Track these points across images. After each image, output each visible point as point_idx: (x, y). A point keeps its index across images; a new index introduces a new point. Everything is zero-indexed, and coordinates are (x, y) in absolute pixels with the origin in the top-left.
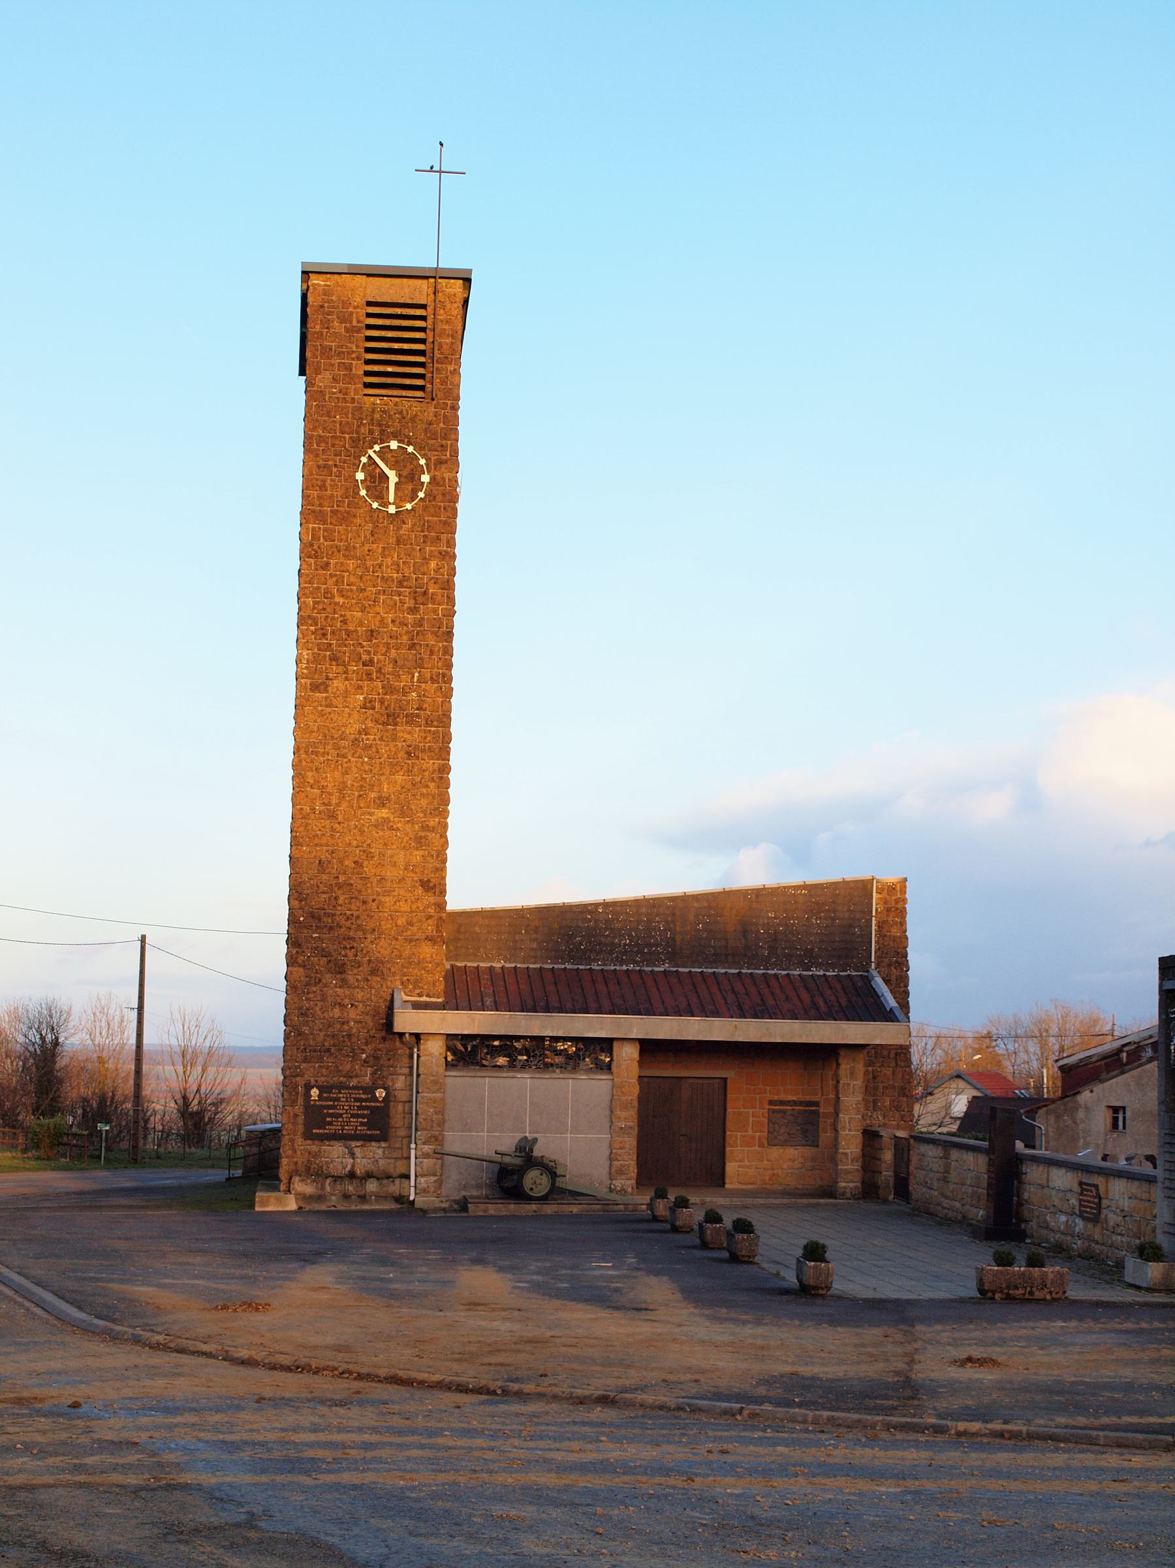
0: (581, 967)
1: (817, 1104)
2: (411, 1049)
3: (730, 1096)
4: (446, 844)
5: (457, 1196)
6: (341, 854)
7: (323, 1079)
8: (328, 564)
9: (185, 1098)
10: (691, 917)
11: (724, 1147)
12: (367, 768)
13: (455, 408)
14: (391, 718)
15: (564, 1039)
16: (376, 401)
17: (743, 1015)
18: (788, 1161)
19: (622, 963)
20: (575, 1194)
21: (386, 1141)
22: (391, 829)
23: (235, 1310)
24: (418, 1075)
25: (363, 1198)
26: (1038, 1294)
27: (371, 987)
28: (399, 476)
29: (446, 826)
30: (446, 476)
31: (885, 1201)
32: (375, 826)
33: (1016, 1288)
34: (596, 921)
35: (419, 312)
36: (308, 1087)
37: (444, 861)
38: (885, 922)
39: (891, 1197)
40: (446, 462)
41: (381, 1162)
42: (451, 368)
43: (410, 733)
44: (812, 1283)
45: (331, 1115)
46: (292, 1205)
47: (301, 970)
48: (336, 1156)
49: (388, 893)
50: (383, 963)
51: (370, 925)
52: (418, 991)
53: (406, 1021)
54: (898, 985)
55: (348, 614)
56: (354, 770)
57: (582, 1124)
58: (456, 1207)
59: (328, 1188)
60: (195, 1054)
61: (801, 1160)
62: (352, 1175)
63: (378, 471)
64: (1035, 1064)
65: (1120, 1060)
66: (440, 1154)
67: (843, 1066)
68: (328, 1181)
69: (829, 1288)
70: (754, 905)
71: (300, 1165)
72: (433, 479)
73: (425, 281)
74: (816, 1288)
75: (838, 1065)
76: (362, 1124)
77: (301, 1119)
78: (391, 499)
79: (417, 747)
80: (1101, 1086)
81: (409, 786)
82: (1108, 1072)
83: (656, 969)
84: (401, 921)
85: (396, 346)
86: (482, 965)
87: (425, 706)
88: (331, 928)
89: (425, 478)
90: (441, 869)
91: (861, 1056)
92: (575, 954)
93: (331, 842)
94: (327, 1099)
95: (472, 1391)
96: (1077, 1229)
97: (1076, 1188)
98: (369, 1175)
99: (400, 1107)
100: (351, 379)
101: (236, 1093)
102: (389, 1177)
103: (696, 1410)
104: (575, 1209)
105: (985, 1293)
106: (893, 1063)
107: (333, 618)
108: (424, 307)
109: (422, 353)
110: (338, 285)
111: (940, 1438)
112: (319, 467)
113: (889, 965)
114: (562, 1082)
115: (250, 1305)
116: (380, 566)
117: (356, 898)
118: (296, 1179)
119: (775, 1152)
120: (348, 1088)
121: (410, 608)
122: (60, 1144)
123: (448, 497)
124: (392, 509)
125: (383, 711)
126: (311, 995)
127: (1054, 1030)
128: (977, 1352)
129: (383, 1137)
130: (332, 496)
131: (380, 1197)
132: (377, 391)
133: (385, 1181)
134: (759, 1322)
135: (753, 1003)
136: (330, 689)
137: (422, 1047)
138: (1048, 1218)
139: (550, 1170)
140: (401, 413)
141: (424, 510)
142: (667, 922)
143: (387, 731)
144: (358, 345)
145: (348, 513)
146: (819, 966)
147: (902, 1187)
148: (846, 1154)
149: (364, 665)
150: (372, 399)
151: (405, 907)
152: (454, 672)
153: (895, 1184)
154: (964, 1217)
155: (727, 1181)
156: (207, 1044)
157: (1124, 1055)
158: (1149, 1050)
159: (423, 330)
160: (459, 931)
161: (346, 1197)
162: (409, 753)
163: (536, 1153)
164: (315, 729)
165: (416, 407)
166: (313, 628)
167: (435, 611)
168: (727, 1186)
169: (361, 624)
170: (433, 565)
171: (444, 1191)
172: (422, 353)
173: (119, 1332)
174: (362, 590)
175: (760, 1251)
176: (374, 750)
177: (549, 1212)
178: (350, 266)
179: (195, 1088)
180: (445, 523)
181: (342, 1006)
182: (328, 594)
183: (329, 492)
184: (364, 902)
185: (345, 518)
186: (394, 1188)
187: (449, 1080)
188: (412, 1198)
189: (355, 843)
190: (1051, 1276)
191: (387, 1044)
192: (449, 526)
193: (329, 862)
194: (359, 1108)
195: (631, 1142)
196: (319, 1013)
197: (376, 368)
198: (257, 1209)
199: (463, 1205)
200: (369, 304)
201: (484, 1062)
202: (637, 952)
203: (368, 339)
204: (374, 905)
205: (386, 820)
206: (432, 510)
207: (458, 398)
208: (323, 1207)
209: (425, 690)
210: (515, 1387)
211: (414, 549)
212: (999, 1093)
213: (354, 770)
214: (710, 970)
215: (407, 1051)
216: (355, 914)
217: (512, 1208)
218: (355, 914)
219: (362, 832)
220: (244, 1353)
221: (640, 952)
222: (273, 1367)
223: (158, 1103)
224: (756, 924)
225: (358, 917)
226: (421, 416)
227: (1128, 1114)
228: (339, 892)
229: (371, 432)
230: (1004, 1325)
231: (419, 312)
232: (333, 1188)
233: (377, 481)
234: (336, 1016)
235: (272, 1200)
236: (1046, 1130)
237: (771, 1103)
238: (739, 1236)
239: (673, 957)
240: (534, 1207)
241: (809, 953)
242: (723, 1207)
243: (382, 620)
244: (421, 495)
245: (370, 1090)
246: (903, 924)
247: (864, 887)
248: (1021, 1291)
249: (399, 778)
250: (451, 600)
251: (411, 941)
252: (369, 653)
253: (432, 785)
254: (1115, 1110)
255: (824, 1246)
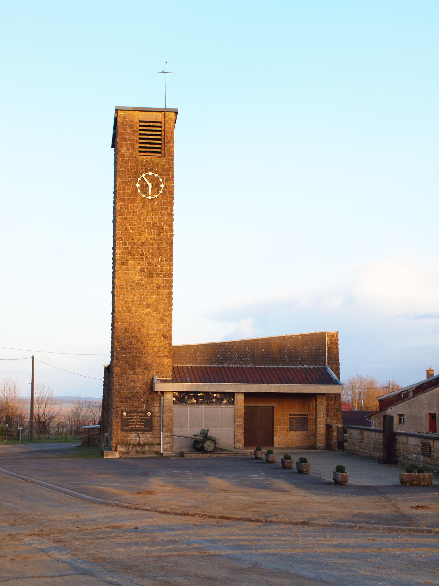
0: (220, 366)
1: (307, 415)
2: (160, 397)
3: (275, 413)
4: (171, 321)
5: (178, 451)
6: (133, 325)
7: (128, 409)
8: (126, 218)
9: (39, 416)
10: (260, 347)
11: (273, 432)
12: (142, 293)
13: (172, 160)
14: (151, 275)
15: (216, 393)
16: (144, 157)
17: (282, 383)
18: (296, 436)
19: (235, 364)
20: (222, 450)
21: (151, 431)
22: (151, 316)
23: (144, 494)
24: (163, 407)
25: (143, 453)
26: (422, 483)
27: (145, 374)
28: (152, 185)
29: (171, 315)
30: (170, 185)
31: (335, 451)
32: (146, 315)
33: (414, 481)
34: (225, 349)
35: (159, 125)
36: (122, 412)
37: (171, 328)
38: (330, 348)
39: (336, 449)
40: (170, 180)
41: (150, 439)
42: (171, 145)
43: (158, 280)
44: (341, 480)
45: (131, 422)
46: (117, 456)
47: (119, 368)
48: (133, 437)
49: (150, 340)
50: (149, 365)
51: (144, 351)
52: (162, 376)
53: (159, 387)
54: (336, 371)
55: (134, 236)
56: (137, 294)
57: (224, 423)
58: (178, 455)
59: (131, 449)
60: (42, 400)
61: (301, 436)
62: (139, 444)
63: (144, 183)
64: (350, 399)
65: (401, 397)
66: (172, 436)
67: (318, 401)
68: (130, 447)
69: (347, 482)
70: (283, 342)
71: (119, 441)
72: (165, 186)
73: (161, 113)
74: (342, 482)
75: (316, 401)
76: (142, 425)
77: (120, 424)
78: (150, 193)
79: (160, 286)
80: (395, 407)
81: (158, 300)
82: (397, 402)
83: (248, 366)
84: (156, 350)
85: (150, 137)
86: (184, 365)
87: (163, 270)
88: (130, 353)
89: (162, 186)
90: (170, 331)
91: (325, 398)
92: (218, 361)
93: (129, 321)
94: (129, 416)
95: (253, 521)
96: (421, 459)
97: (420, 444)
98: (145, 444)
99: (156, 419)
100: (134, 149)
101: (57, 415)
102: (153, 445)
103: (338, 526)
104: (224, 455)
105: (403, 483)
106: (334, 400)
107: (129, 238)
108: (160, 123)
109: (160, 140)
110: (129, 114)
111: (430, 534)
112: (123, 182)
113: (333, 364)
114: (216, 408)
115: (149, 492)
116: (146, 218)
117: (139, 342)
118: (119, 446)
119: (292, 433)
120: (137, 412)
121: (157, 234)
122: (4, 434)
123: (171, 193)
124: (150, 198)
125: (148, 272)
126: (123, 378)
127: (357, 386)
128: (420, 504)
129: (150, 430)
130: (127, 193)
131: (150, 452)
132: (144, 154)
133: (152, 446)
134: (331, 495)
135: (282, 379)
136: (128, 264)
137: (165, 396)
138: (408, 455)
139: (213, 440)
140: (153, 162)
141: (162, 198)
142: (251, 349)
143: (149, 279)
144: (136, 137)
145: (134, 199)
146: (307, 364)
147: (341, 445)
148: (320, 433)
149: (141, 255)
150: (142, 157)
151: (157, 345)
152: (174, 257)
153: (338, 444)
154: (370, 456)
155: (275, 444)
156: (47, 396)
157: (402, 395)
158: (411, 393)
159: (160, 131)
160: (175, 353)
161: (137, 452)
162: (157, 288)
163: (209, 435)
164: (123, 279)
165: (158, 160)
166: (121, 242)
167: (166, 235)
168: (275, 446)
169: (139, 240)
170: (165, 218)
171: (173, 450)
172: (160, 140)
173: (109, 503)
174: (139, 228)
175: (310, 470)
176: (145, 286)
177: (214, 457)
178: (133, 107)
179: (42, 412)
180: (170, 202)
181: (134, 382)
182: (127, 229)
183: (126, 191)
184: (142, 343)
185: (133, 201)
186: (155, 449)
187: (174, 408)
188: (162, 452)
189: (138, 321)
190: (427, 476)
191: (151, 396)
192: (171, 204)
193: (129, 328)
194: (141, 419)
195: (242, 430)
196: (126, 384)
197: (143, 145)
198: (105, 457)
199: (182, 454)
200: (140, 121)
201: (187, 402)
202: (241, 360)
203: (140, 134)
204: (146, 344)
205: (149, 313)
206: (165, 198)
207: (173, 156)
208: (129, 456)
209: (163, 264)
210: (270, 519)
211: (158, 212)
212: (348, 410)
213: (137, 294)
214: (267, 366)
215: (159, 398)
216: (139, 347)
217: (201, 455)
218: (139, 347)
219: (141, 317)
220: (162, 509)
221: (242, 360)
222: (176, 514)
223: (27, 418)
224: (284, 349)
225: (140, 349)
226: (160, 163)
227: (405, 417)
228: (133, 340)
229: (142, 169)
230: (417, 494)
231: (159, 125)
232: (132, 449)
233: (144, 187)
234: (132, 385)
235: (110, 454)
236: (375, 423)
237: (290, 415)
238: (303, 464)
239: (253, 362)
240: (209, 455)
241: (303, 359)
242: (291, 453)
243: (147, 238)
244: (161, 192)
245: (145, 413)
246: (337, 348)
247: (323, 335)
248: (416, 482)
249: (154, 297)
250: (172, 231)
251: (159, 357)
252: (142, 251)
253: (166, 299)
254: (400, 415)
255: (344, 467)
